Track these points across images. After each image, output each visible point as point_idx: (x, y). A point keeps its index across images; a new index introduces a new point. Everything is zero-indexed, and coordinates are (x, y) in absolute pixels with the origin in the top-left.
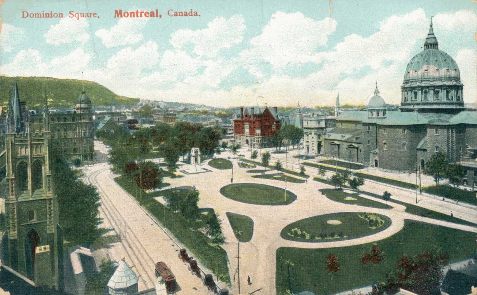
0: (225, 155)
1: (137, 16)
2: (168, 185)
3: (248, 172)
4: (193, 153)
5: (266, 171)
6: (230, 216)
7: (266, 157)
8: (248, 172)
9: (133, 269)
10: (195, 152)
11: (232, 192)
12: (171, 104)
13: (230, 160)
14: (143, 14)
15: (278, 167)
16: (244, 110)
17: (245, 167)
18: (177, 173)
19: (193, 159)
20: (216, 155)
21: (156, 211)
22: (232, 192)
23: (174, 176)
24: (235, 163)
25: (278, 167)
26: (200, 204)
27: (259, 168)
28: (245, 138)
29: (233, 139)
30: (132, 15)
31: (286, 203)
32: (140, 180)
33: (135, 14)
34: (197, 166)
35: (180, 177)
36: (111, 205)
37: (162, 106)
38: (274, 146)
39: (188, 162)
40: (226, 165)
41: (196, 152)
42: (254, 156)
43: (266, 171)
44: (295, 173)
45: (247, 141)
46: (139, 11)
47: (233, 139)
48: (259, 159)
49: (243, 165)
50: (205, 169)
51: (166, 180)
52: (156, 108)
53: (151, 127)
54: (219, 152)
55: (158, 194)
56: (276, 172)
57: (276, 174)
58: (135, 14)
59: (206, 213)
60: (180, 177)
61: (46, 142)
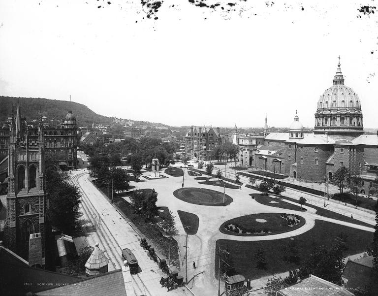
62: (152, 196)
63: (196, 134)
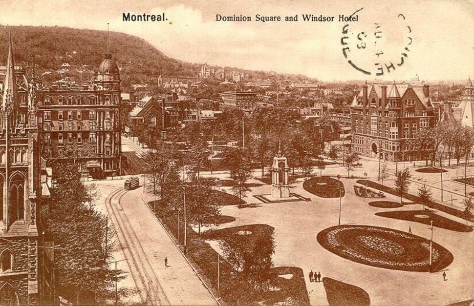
0: (333, 170)
1: (145, 20)
2: (232, 219)
3: (371, 204)
4: (276, 166)
5: (403, 204)
6: (329, 284)
7: (402, 178)
8: (371, 204)
9: (126, 251)
10: (279, 164)
11: (345, 240)
12: (251, 76)
13: (340, 180)
14: (150, 18)
15: (423, 198)
16: (369, 90)
17: (366, 196)
18: (249, 197)
19: (275, 177)
20: (316, 171)
21: (205, 264)
22: (345, 240)
23: (241, 204)
24: (349, 185)
25: (423, 198)
26: (278, 259)
27: (391, 198)
28: (371, 141)
29: (349, 142)
30: (140, 18)
31: (434, 268)
32: (183, 208)
33: (143, 17)
34: (283, 189)
35: (254, 206)
36: (131, 232)
37: (237, 79)
38: (423, 159)
39: (267, 180)
40: (330, 188)
41: (281, 164)
42: (383, 175)
43: (403, 204)
44: (455, 212)
45: (374, 147)
46: (146, 15)
47: (349, 142)
48: (391, 183)
49: (362, 193)
50: (296, 195)
51: (226, 210)
52: (226, 82)
53: (215, 115)
54: (322, 165)
55: (213, 235)
56: (420, 207)
57: (419, 212)
58: (143, 17)
59: (289, 276)
60: (254, 206)
61: (31, 144)
62: (262, 240)
63: (374, 101)
